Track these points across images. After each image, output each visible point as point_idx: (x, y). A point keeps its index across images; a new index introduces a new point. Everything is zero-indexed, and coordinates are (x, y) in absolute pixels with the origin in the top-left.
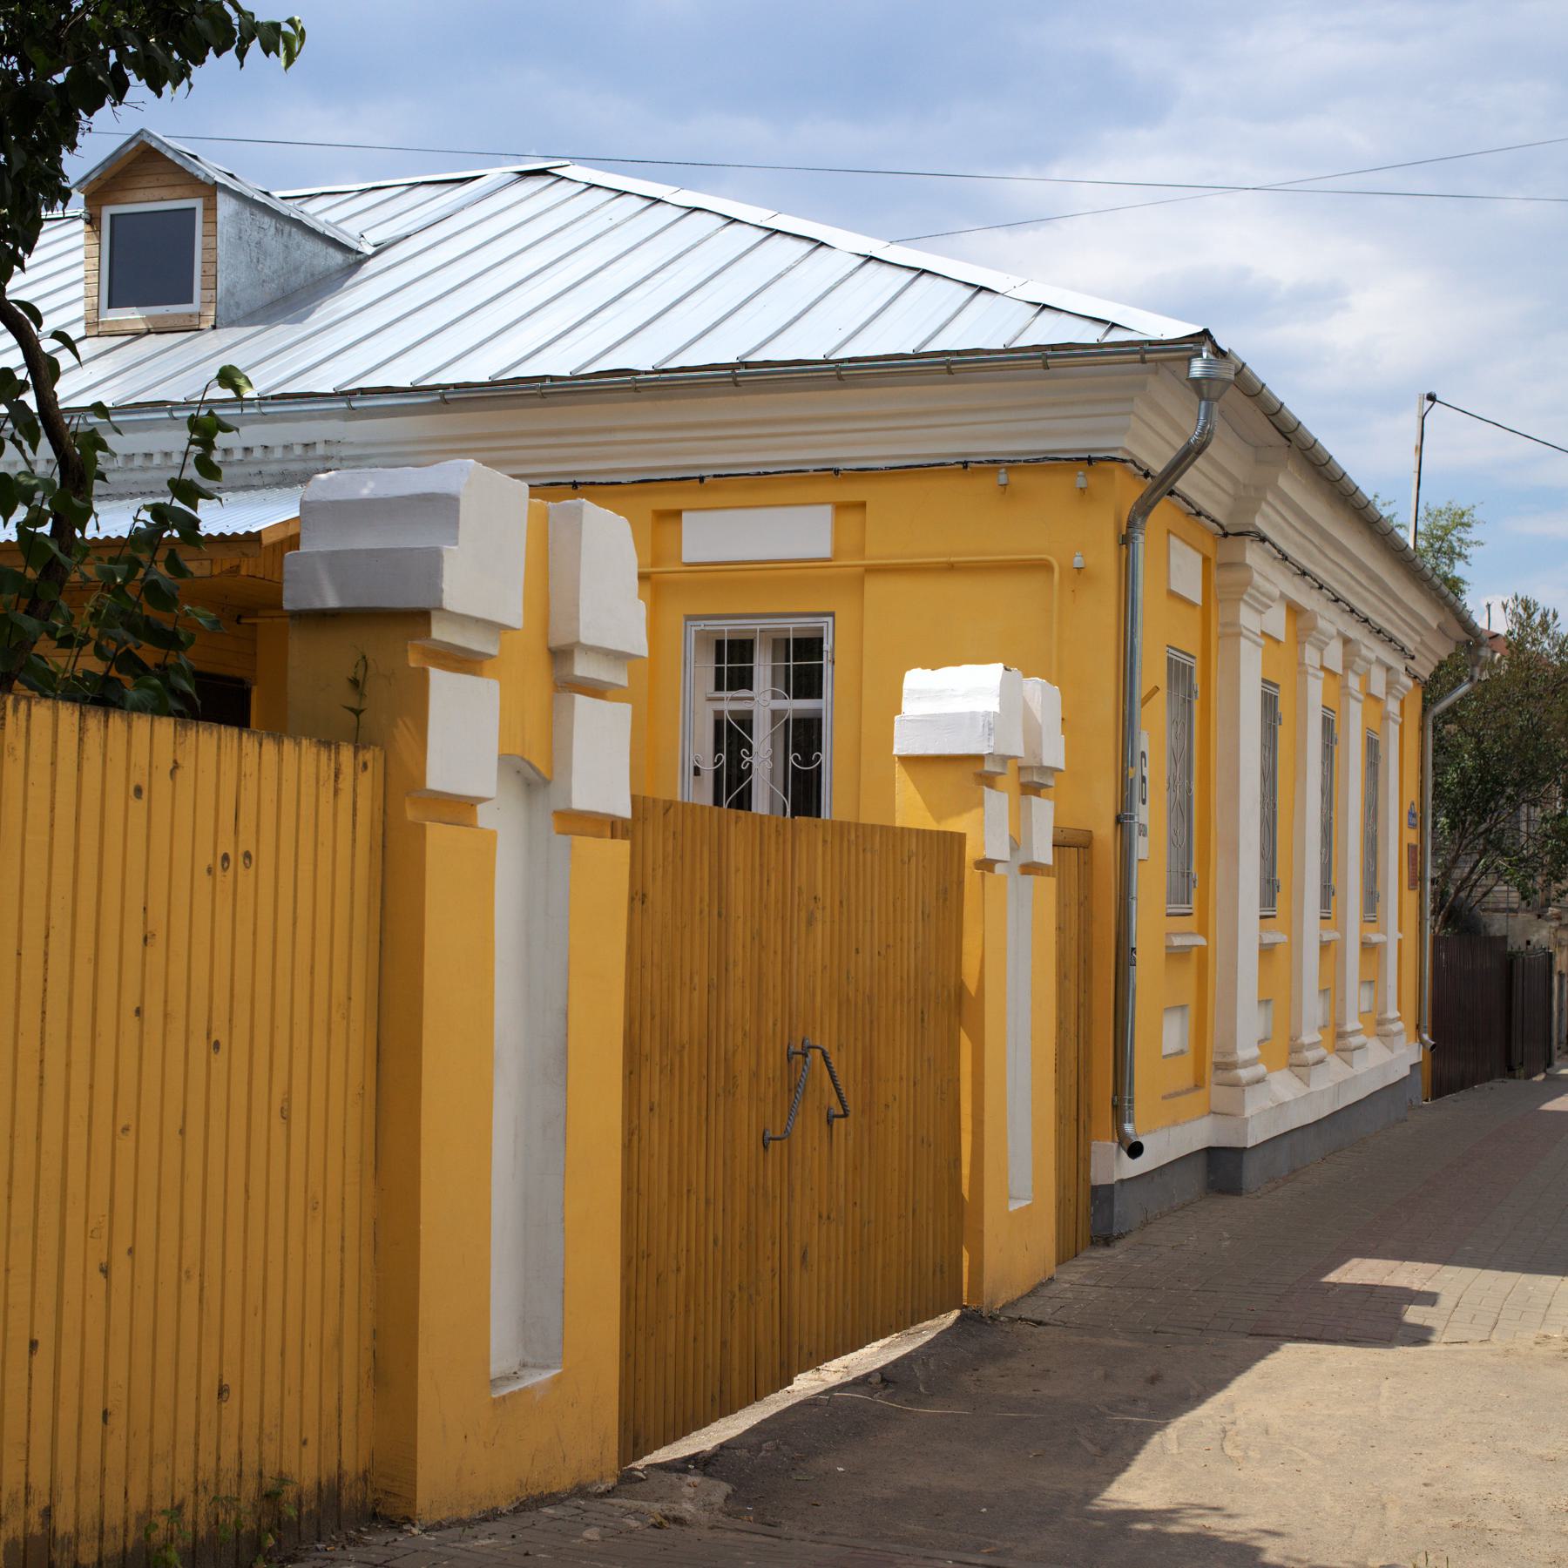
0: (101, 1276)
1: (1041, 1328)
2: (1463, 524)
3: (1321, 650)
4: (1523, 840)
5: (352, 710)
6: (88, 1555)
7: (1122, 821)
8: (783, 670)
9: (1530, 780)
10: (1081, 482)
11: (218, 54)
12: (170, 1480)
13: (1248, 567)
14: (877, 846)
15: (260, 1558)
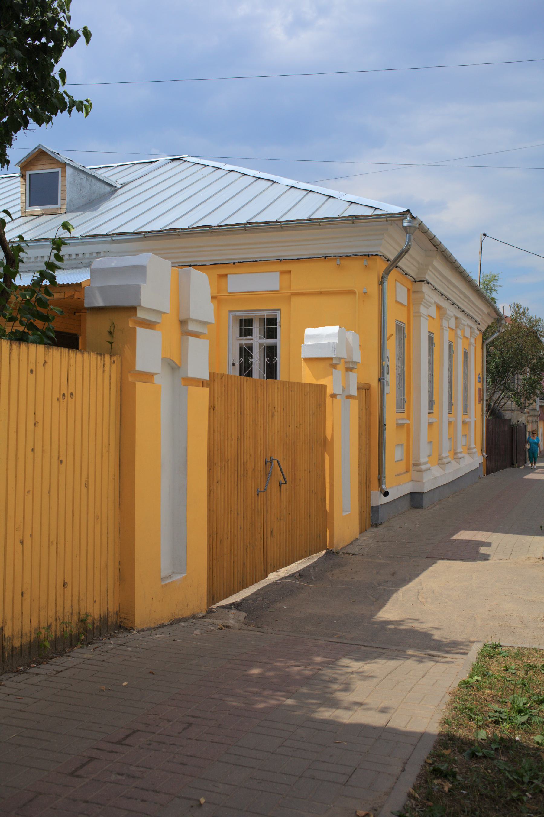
0: (20, 544)
1: (354, 556)
2: (495, 280)
3: (448, 321)
4: (516, 386)
5: (109, 342)
6: (17, 644)
7: (381, 380)
8: (263, 329)
9: (519, 365)
10: (366, 263)
11: (61, 112)
12: (46, 616)
13: (423, 292)
14: (296, 390)
15: (79, 643)
